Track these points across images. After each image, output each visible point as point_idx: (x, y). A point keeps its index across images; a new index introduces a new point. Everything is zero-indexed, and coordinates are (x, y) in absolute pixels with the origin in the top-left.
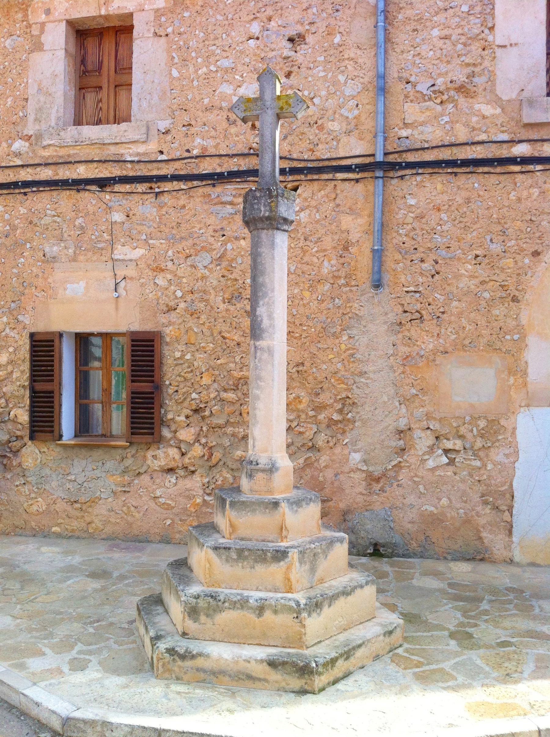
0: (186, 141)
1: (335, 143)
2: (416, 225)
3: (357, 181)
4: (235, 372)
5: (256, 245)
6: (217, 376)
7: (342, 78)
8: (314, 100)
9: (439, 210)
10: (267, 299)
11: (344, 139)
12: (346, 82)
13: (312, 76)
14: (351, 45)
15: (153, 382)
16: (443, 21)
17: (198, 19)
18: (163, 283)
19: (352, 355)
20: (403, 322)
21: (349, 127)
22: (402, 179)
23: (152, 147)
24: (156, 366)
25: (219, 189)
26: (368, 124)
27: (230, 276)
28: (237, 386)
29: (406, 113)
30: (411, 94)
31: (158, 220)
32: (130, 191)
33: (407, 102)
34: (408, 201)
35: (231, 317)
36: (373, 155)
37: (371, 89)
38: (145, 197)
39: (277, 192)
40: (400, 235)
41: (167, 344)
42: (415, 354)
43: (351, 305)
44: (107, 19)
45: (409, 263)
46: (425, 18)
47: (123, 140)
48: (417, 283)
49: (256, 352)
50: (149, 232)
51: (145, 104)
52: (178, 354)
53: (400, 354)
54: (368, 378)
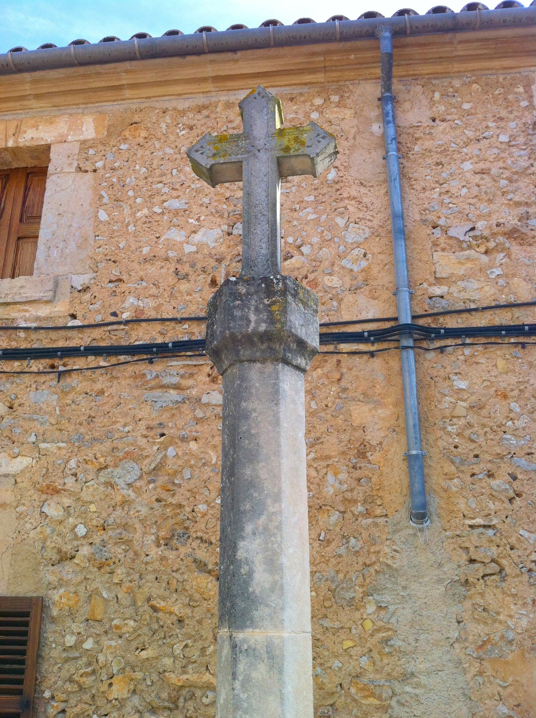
0: (112, 302)
1: (335, 304)
2: (472, 418)
3: (372, 354)
4: (172, 675)
5: (234, 397)
6: (138, 682)
7: (341, 222)
8: (302, 249)
9: (505, 397)
10: (263, 519)
11: (349, 298)
12: (347, 227)
13: (298, 220)
14: (351, 182)
15: (20, 692)
16: (476, 152)
17: (140, 153)
18: (56, 513)
19: (386, 641)
20: (471, 580)
21: (355, 282)
22: (442, 352)
23: (59, 309)
24: (29, 662)
25: (158, 367)
26: (383, 279)
27: (170, 500)
28: (175, 702)
29: (437, 265)
30: (442, 241)
31: (58, 412)
32: (18, 370)
33: (436, 251)
34: (455, 383)
35: (169, 570)
36: (396, 319)
37: (383, 234)
38: (42, 378)
39: (285, 284)
40: (449, 434)
41: (53, 620)
42: (497, 638)
43: (377, 548)
44: (15, 155)
45: (469, 479)
46: (451, 149)
47: (18, 299)
48: (486, 512)
49: (235, 661)
50: (41, 432)
51: (55, 253)
52: (70, 640)
53: (470, 638)
54: (418, 685)
